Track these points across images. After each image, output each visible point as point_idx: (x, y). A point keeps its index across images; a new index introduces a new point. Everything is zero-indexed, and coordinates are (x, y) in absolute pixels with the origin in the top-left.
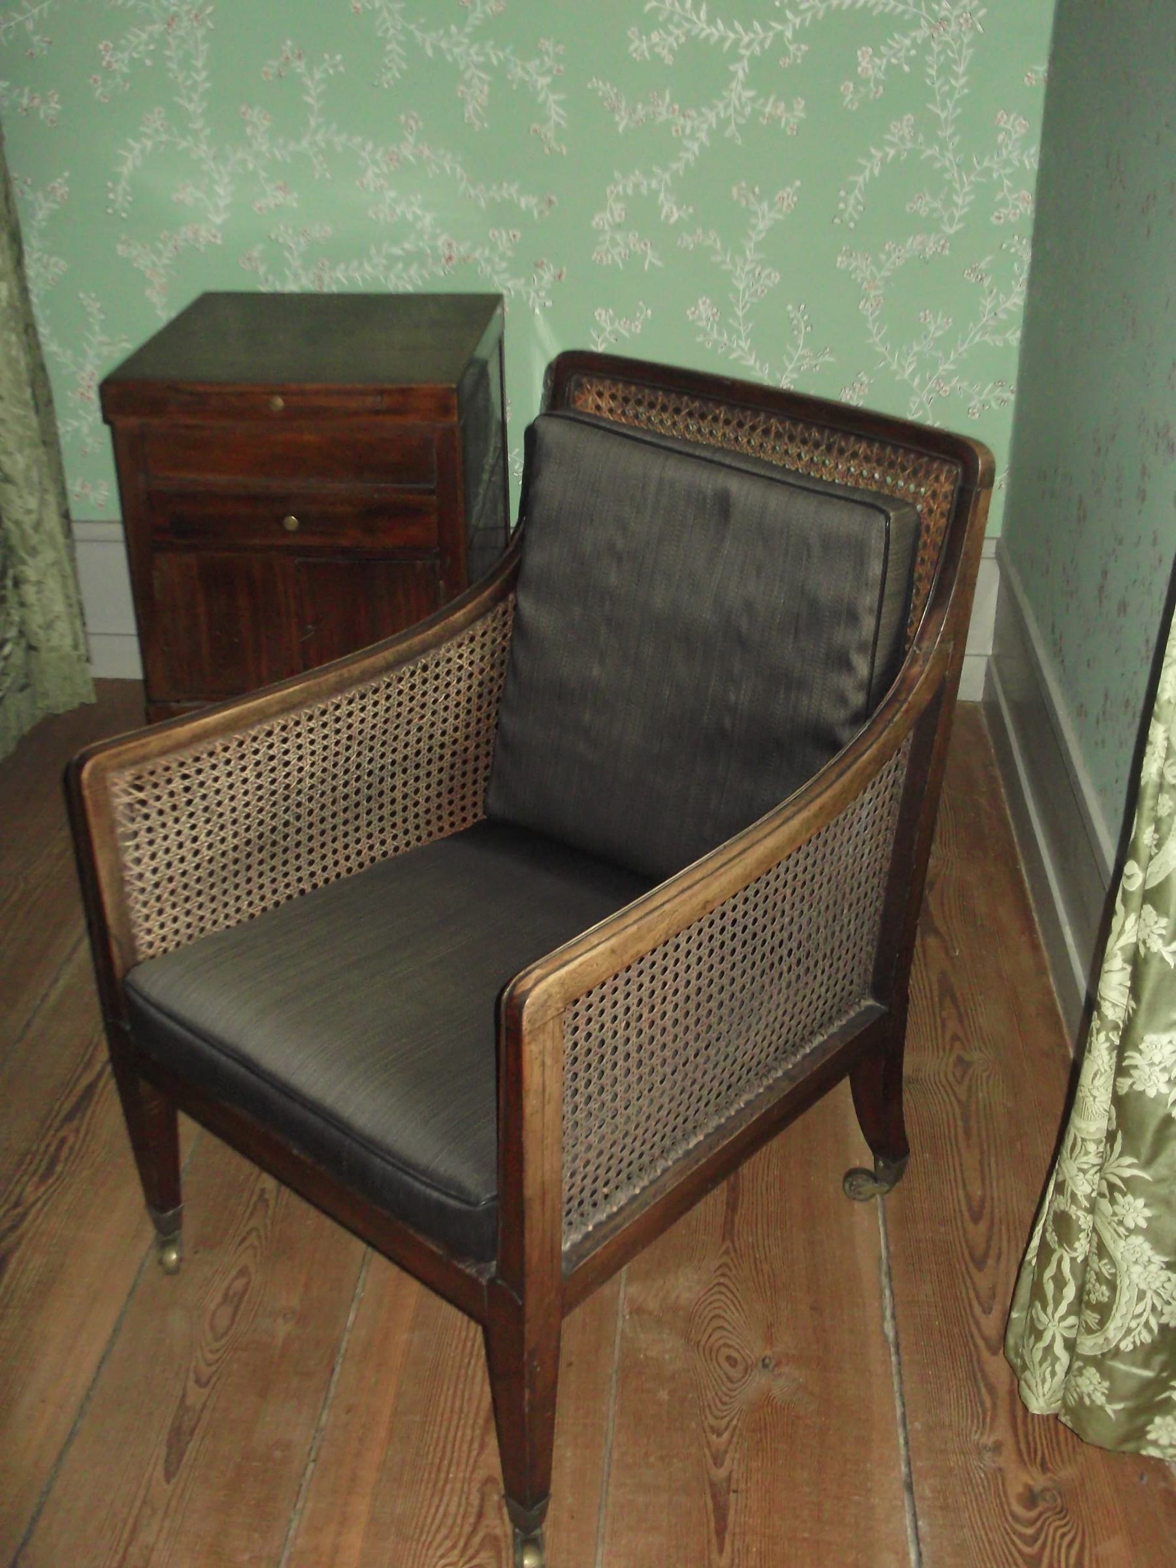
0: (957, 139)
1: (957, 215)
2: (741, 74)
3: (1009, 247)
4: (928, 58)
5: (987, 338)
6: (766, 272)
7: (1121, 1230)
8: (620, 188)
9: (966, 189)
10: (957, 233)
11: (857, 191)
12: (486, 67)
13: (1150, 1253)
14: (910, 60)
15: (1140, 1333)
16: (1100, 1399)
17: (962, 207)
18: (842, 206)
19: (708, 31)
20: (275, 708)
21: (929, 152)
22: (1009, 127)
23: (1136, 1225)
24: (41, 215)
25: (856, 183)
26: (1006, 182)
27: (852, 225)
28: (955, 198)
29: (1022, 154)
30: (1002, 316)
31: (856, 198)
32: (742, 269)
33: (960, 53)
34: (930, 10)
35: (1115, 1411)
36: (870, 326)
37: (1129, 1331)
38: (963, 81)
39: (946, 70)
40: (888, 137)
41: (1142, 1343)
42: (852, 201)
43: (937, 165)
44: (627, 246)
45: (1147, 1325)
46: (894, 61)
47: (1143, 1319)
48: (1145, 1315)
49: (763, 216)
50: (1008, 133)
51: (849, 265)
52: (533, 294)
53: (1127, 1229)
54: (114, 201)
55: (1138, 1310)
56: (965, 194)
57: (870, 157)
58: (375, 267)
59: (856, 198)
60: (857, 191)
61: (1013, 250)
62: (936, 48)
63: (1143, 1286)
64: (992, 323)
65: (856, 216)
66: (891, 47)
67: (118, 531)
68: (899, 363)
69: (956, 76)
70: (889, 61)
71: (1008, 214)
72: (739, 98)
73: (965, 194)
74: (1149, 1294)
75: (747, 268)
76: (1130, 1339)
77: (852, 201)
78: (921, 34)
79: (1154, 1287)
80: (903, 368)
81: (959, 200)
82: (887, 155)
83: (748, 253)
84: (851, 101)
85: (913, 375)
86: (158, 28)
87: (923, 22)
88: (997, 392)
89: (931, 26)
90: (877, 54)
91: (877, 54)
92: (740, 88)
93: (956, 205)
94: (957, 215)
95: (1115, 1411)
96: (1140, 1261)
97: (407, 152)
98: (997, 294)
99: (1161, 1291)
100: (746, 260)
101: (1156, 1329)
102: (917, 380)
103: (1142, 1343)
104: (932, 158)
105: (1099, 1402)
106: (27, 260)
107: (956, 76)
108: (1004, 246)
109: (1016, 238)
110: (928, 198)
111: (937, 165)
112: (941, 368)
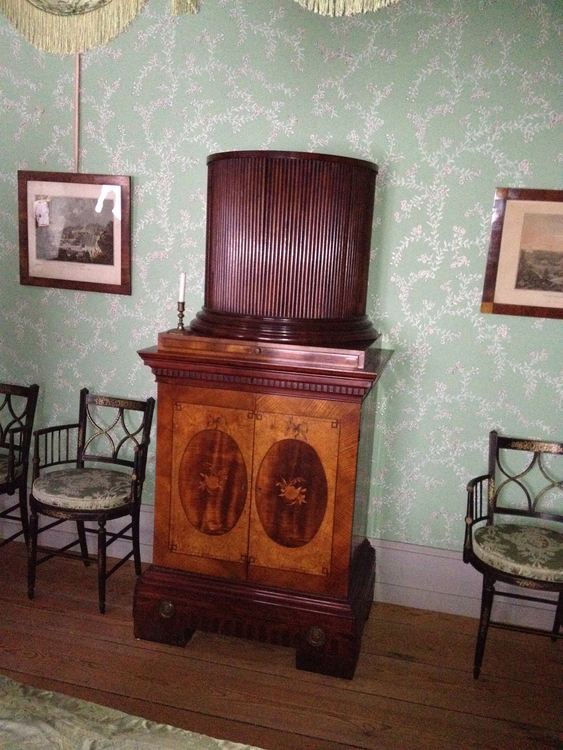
0: (438, 235)
2: (372, 40)
3: (459, 277)
4: (428, 205)
5: (449, 312)
6: (379, 119)
8: (323, 85)
9: (441, 254)
10: (438, 270)
12: (276, 38)
14: (421, 205)
19: (361, 24)
21: (427, 240)
22: (440, 387)
24: (105, 381)
25: (399, 249)
26: (457, 252)
29: (445, 396)
30: (455, 304)
33: (458, 31)
34: (447, 16)
36: (419, 143)
38: (441, 214)
39: (434, 210)
40: (411, 233)
42: (397, 256)
43: (430, 244)
46: (432, 35)
50: (440, 389)
52: (287, 128)
54: (130, 380)
56: (460, 88)
57: (404, 240)
58: (228, 116)
60: (416, 87)
61: (479, 112)
62: (431, 201)
64: (451, 306)
65: (398, 261)
66: (414, 201)
68: (414, 320)
69: (438, 212)
70: (397, 361)
72: (371, 50)
75: (371, 118)
77: (397, 256)
78: (425, 196)
80: (415, 321)
81: (438, 258)
82: (428, 72)
84: (398, 219)
85: (419, 325)
86: (155, 182)
87: (409, 349)
88: (436, 481)
89: (412, 350)
90: (409, 203)
91: (409, 203)
92: (372, 46)
93: (437, 260)
97: (243, 71)
100: (371, 114)
102: (420, 327)
104: (429, 242)
106: (102, 173)
107: (438, 212)
110: (444, 90)
111: (430, 244)
112: (448, 162)
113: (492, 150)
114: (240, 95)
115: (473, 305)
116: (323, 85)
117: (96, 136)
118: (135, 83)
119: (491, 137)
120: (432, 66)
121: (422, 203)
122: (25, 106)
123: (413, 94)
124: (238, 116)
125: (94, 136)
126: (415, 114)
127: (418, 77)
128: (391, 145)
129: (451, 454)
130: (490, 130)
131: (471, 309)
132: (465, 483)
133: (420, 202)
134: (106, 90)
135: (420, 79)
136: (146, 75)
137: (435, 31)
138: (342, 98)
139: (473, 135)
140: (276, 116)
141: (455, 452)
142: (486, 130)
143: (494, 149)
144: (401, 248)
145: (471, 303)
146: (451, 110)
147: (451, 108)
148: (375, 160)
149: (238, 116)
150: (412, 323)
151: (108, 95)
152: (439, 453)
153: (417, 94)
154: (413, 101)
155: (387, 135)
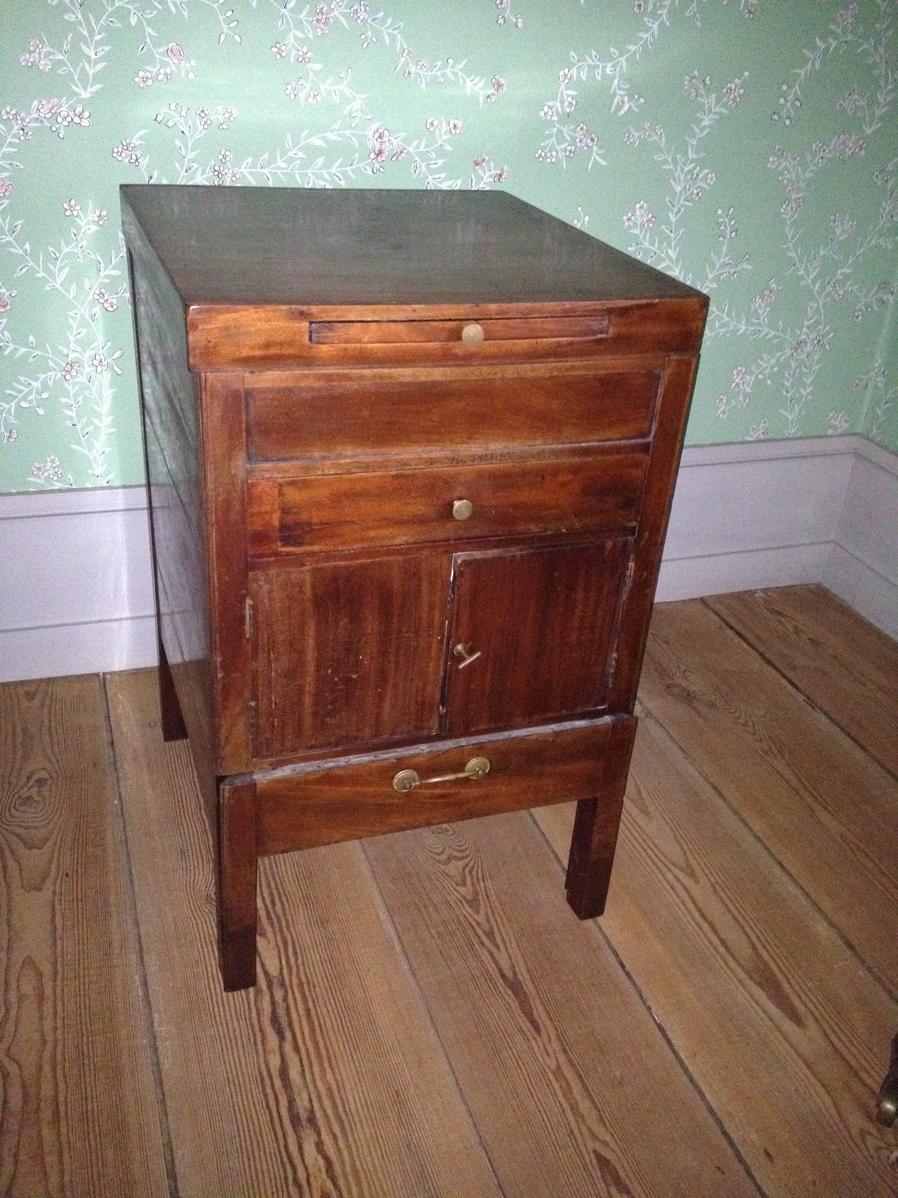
1: (91, 72)
11: (797, 86)
31: (796, 93)
58: (290, 161)
69: (804, 385)
73: (99, 43)
107: (804, 385)
114: (329, 93)
116: (574, 71)
117: (652, 243)
118: (785, 87)
120: (839, 31)
122: (441, 152)
124: (321, 161)
125: (647, 244)
127: (806, 61)
134: (701, 107)
135: (809, 66)
136: (817, 66)
137: (30, 393)
140: (440, 162)
147: (79, 110)
148: (685, 277)
149: (321, 161)
151: (706, 123)
153: (798, 104)
155: (720, 212)
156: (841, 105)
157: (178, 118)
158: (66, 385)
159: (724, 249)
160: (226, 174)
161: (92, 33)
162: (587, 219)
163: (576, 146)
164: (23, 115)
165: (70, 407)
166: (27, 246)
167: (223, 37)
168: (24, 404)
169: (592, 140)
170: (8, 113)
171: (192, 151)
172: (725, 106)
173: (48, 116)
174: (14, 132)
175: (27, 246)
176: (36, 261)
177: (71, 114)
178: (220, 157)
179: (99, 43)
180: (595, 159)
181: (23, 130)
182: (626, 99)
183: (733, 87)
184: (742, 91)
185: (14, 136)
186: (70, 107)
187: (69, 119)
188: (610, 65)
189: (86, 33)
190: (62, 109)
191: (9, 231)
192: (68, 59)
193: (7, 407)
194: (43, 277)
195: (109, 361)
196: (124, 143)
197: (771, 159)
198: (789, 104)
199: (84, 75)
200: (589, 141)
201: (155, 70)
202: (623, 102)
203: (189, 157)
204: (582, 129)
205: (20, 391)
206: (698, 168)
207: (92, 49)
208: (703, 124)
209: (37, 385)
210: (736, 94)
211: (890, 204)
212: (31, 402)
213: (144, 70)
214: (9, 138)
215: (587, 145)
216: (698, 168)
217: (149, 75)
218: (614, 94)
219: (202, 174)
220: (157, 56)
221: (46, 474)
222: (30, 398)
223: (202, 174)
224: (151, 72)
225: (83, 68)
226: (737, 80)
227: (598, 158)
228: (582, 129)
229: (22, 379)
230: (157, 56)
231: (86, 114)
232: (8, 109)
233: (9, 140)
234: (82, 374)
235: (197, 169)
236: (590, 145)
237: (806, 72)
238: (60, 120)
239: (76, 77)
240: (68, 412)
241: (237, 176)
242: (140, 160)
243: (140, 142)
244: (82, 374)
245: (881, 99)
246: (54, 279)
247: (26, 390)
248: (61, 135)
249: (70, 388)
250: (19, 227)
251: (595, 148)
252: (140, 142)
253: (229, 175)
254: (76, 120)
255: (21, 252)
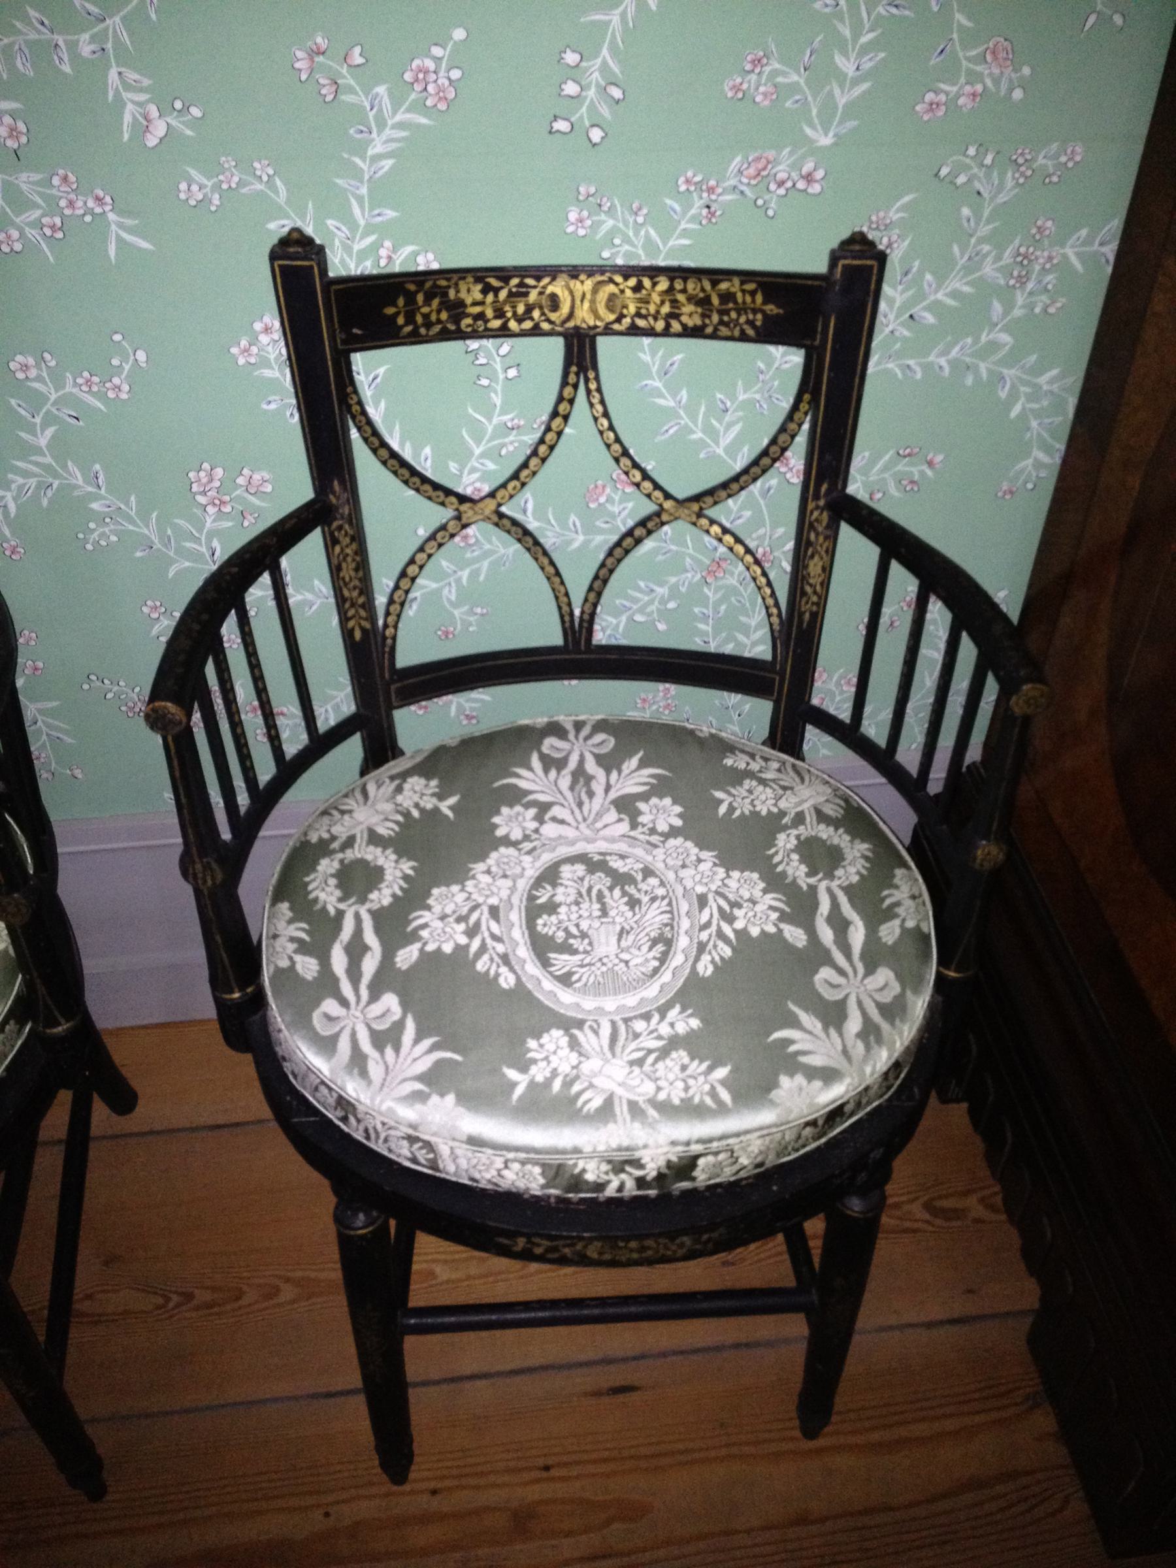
1: (842, 100)
7: (655, 839)
11: (605, 52)
13: (696, 850)
15: (715, 946)
16: (429, 803)
17: (855, 82)
18: (571, 88)
20: (517, 1308)
23: (671, 826)
27: (596, 135)
28: (839, 60)
31: (604, 68)
32: (348, 249)
35: (451, 808)
37: (702, 948)
41: (722, 958)
44: (52, 206)
45: (721, 935)
47: (714, 928)
48: (715, 922)
49: (381, 124)
51: (596, 226)
53: (661, 834)
55: (705, 916)
59: (604, 68)
61: (961, 179)
63: (700, 889)
65: (605, 111)
67: (339, 1266)
71: (958, 96)
73: (864, 50)
74: (710, 896)
76: (706, 958)
79: (713, 888)
83: (357, 211)
93: (841, 77)
94: (842, 100)
95: (451, 808)
96: (688, 862)
98: (921, 273)
99: (724, 890)
100: (353, 225)
101: (731, 935)
103: (722, 958)
105: (429, 806)
108: (944, 171)
109: (972, 151)
113: (1003, 362)
115: (1018, 312)
119: (1009, 306)
121: (672, 605)
123: (592, 93)
126: (611, 212)
128: (493, 378)
129: (997, 307)
130: (1007, 272)
131: (1005, 338)
132: (1047, 449)
133: (663, 601)
137: (651, 602)
138: (152, 141)
139: (920, 296)
141: (1020, 299)
142: (988, 269)
143: (1012, 359)
144: (616, 19)
145: (1009, 306)
146: (809, 178)
147: (808, 167)
150: (702, 444)
152: (930, 319)
153: (617, 93)
154: (596, 135)
156: (736, 88)
157: (976, 170)
158: (706, 590)
159: (498, 400)
160: (1037, 258)
161: (857, 34)
162: (141, 356)
163: (62, 216)
164: (712, 183)
165: (705, 618)
166: (684, 393)
167: (1092, 19)
168: (639, 618)
169: (99, 199)
170: (688, 181)
171: (988, 222)
172: (420, 107)
173: (753, 182)
174: (693, 211)
175: (684, 393)
176: (693, 417)
177: (794, 175)
178: (1034, 231)
179: (864, 50)
180: (118, 238)
181: (708, 207)
182: (153, 111)
183: (430, 64)
184: (456, 74)
185: (693, 219)
186: (793, 166)
187: (789, 184)
188: (86, 37)
189: (847, 33)
190: (781, 167)
191: (658, 372)
192: (807, 82)
193: (614, 621)
194: (701, 439)
195: (776, 554)
196: (874, 218)
197: (573, 216)
198: (592, 93)
199: (828, 106)
200: (91, 204)
201: (955, 89)
202: (146, 117)
203: (979, 234)
204: (65, 179)
205: (635, 600)
206: (387, 244)
207: (852, 60)
208: (370, 152)
209: (661, 591)
210: (443, 81)
211: (903, 292)
212: (650, 614)
213: (937, 92)
214: (683, 223)
215: (91, 212)
216: (387, 244)
217: (943, 98)
218: (120, 104)
219: (994, 263)
220: (964, 63)
221: (654, 707)
222: (649, 610)
223: (994, 263)
224: (947, 93)
225: (831, 94)
226: (437, 51)
227: (125, 235)
228: (65, 179)
229: (642, 584)
230: (964, 63)
231: (820, 174)
232: (690, 174)
233: (683, 225)
234: (732, 574)
235: (988, 253)
236: (98, 210)
237: (623, 15)
238: (773, 187)
239: (814, 112)
240: (702, 626)
241: (1055, 261)
242: (895, 245)
243: (900, 215)
244: (732, 574)
245: (847, 66)
246: (717, 444)
247: (646, 598)
248: (770, 213)
249: (710, 594)
250: (675, 366)
251: (112, 216)
252: (900, 215)
253: (1041, 261)
254: (801, 185)
255: (672, 404)
